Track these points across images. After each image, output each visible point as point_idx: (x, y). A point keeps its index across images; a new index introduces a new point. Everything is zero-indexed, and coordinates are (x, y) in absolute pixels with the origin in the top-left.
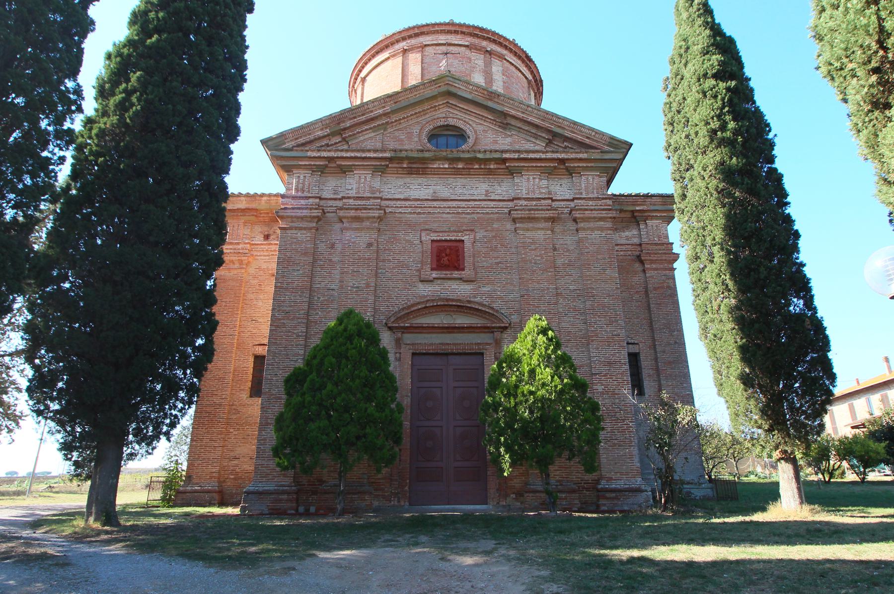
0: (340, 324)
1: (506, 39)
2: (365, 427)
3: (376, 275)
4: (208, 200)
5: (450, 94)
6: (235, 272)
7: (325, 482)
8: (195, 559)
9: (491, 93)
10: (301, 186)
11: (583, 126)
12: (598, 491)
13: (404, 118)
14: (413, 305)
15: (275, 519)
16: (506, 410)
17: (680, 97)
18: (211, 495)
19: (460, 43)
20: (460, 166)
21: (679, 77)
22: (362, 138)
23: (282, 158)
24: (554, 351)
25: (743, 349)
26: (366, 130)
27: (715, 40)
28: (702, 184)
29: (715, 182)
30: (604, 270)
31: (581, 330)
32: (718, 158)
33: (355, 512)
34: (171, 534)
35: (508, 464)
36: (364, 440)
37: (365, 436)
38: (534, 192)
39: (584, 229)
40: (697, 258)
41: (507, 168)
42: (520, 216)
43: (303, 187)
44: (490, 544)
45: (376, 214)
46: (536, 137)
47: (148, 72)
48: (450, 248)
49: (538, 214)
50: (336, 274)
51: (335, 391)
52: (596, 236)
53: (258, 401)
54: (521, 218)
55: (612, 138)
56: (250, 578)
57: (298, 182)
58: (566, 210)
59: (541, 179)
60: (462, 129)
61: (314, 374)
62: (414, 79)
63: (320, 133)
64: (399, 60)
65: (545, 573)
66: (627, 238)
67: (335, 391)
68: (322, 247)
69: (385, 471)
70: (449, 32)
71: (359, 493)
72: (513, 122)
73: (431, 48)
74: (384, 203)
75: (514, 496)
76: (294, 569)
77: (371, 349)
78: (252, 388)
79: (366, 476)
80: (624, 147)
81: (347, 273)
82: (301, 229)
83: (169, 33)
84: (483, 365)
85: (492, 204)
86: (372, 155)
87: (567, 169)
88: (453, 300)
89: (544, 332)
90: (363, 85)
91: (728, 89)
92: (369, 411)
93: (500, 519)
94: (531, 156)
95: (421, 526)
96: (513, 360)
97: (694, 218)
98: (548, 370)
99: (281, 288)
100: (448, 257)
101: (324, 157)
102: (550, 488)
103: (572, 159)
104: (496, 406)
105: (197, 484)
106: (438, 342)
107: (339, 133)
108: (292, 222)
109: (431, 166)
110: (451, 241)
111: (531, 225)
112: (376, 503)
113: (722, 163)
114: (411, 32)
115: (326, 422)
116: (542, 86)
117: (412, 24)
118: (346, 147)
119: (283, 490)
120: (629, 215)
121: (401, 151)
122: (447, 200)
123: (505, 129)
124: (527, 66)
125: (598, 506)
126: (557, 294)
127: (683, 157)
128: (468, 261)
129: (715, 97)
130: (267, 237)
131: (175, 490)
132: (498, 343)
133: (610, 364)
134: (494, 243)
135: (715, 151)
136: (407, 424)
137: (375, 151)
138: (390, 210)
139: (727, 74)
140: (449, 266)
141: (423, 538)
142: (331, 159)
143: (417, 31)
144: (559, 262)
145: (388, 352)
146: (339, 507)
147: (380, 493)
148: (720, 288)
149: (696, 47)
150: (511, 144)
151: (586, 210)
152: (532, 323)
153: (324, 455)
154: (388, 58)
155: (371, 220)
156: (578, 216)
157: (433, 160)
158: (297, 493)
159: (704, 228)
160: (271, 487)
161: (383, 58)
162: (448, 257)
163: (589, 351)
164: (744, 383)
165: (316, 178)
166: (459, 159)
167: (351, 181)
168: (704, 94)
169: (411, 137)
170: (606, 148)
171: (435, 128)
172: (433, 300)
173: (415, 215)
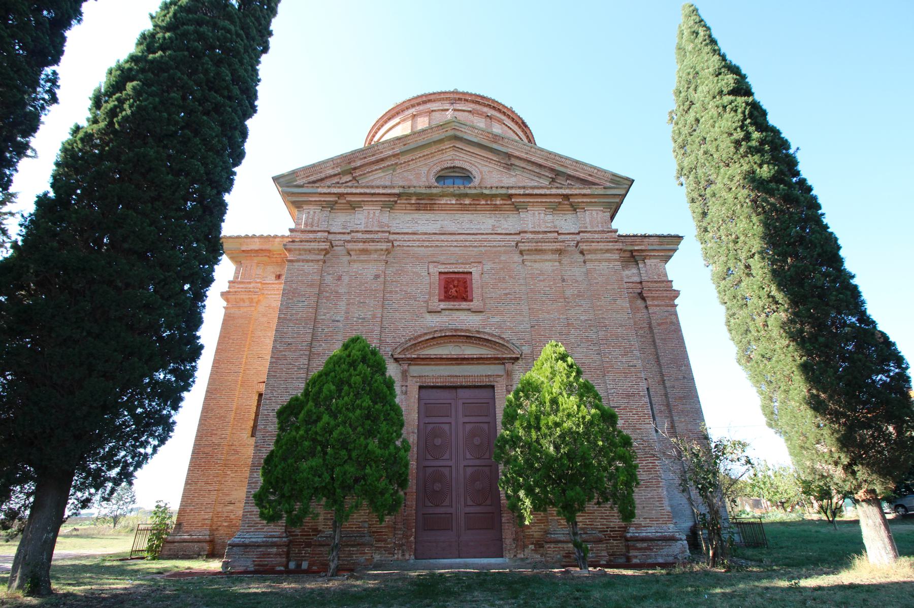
2: (364, 468)
6: (245, 310)
7: (320, 531)
10: (310, 220)
12: (627, 540)
14: (420, 336)
16: (529, 445)
18: (201, 544)
22: (372, 178)
23: (293, 194)
25: (805, 368)
26: (376, 170)
30: (615, 300)
31: (595, 362)
33: (350, 569)
35: (528, 510)
37: (364, 477)
38: (539, 226)
39: (591, 260)
40: (728, 272)
41: (513, 204)
42: (527, 248)
45: (384, 246)
46: (539, 175)
47: (146, 83)
49: (545, 246)
50: (342, 305)
51: (333, 423)
52: (606, 267)
55: (614, 175)
57: (307, 218)
58: (572, 243)
60: (468, 171)
63: (331, 172)
68: (329, 279)
69: (387, 518)
71: (358, 545)
72: (517, 162)
74: (392, 237)
77: (378, 377)
79: (366, 525)
81: (353, 304)
82: (308, 261)
86: (381, 191)
88: (461, 330)
89: (563, 358)
92: (370, 447)
93: (526, 581)
96: (530, 389)
98: (572, 398)
99: (285, 319)
100: (456, 288)
101: (334, 194)
102: (578, 539)
104: (514, 441)
105: (187, 532)
107: (350, 172)
108: (300, 254)
109: (438, 202)
111: (538, 257)
112: (377, 557)
114: (420, 100)
119: (272, 542)
120: (628, 254)
123: (509, 169)
125: (628, 559)
128: (476, 292)
130: (279, 277)
132: (509, 374)
133: (628, 396)
136: (413, 464)
140: (457, 297)
142: (340, 195)
143: (424, 99)
144: (568, 293)
145: (394, 382)
146: (333, 565)
148: (765, 301)
152: (548, 350)
158: (289, 545)
160: (259, 538)
162: (456, 288)
165: (326, 213)
166: (466, 195)
167: (360, 216)
169: (420, 175)
170: (608, 184)
171: (443, 170)
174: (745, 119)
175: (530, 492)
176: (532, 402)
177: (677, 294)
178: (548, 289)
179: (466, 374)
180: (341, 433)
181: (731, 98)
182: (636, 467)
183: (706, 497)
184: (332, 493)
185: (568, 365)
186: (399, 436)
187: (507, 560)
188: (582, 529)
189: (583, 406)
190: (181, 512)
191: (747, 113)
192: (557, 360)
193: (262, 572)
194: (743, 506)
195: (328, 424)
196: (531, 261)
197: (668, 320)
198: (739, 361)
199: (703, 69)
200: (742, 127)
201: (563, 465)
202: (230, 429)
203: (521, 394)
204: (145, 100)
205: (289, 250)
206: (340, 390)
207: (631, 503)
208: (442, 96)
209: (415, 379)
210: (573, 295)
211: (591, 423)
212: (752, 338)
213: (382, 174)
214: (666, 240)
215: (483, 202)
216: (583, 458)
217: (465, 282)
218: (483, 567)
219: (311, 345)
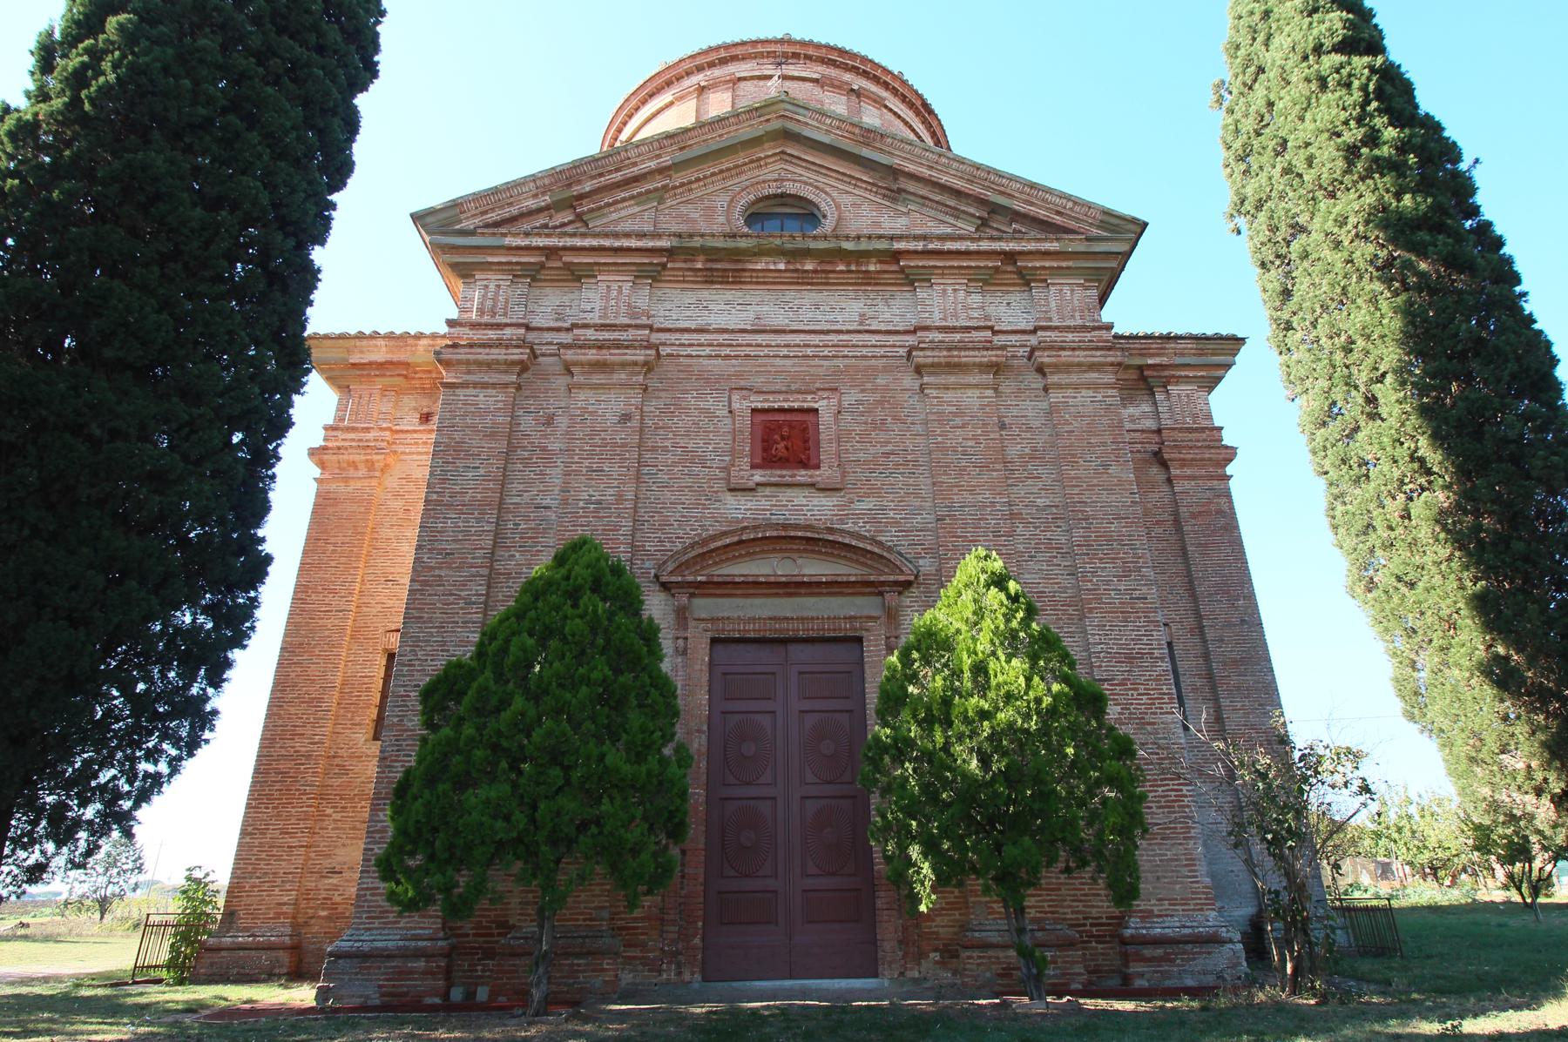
3: (638, 478)
6: (359, 485)
9: (868, 131)
10: (489, 303)
11: (1049, 191)
12: (1124, 942)
13: (698, 180)
14: (713, 538)
16: (928, 756)
18: (274, 954)
19: (804, 74)
20: (809, 267)
22: (614, 216)
24: (1026, 622)
25: (1482, 604)
26: (624, 200)
28: (1337, 258)
29: (1370, 249)
30: (1106, 466)
32: (1370, 199)
38: (955, 315)
39: (1059, 386)
41: (902, 270)
42: (932, 360)
45: (640, 356)
46: (956, 213)
48: (791, 425)
49: (966, 357)
50: (555, 475)
51: (532, 713)
52: (1087, 398)
54: (932, 365)
55: (1108, 213)
61: (488, 673)
63: (531, 203)
67: (532, 713)
68: (527, 423)
69: (647, 901)
71: (589, 953)
72: (911, 186)
73: (749, 83)
79: (605, 914)
80: (1131, 230)
81: (578, 473)
82: (485, 386)
85: (873, 339)
86: (633, 243)
87: (1020, 273)
88: (796, 527)
89: (999, 581)
92: (609, 760)
94: (949, 246)
96: (934, 644)
98: (1015, 662)
99: (439, 503)
100: (785, 441)
101: (538, 248)
102: (1027, 940)
103: (1030, 253)
104: (901, 748)
105: (246, 929)
106: (766, 613)
108: (469, 372)
110: (791, 410)
111: (952, 379)
112: (627, 978)
114: (713, 57)
119: (417, 949)
120: (1133, 375)
121: (691, 236)
122: (783, 332)
123: (894, 200)
124: (924, 122)
125: (1126, 979)
129: (1348, 85)
132: (892, 616)
133: (1130, 658)
137: (641, 235)
138: (668, 350)
139: (1363, 45)
140: (787, 460)
142: (551, 252)
143: (723, 54)
144: (1013, 451)
146: (537, 994)
148: (1406, 468)
152: (971, 567)
154: (672, 103)
155: (630, 369)
156: (1046, 360)
157: (755, 254)
158: (448, 954)
159: (1348, 350)
161: (662, 104)
162: (785, 441)
163: (1085, 632)
165: (522, 288)
166: (807, 253)
167: (591, 295)
168: (1323, 83)
169: (714, 211)
170: (1095, 232)
172: (755, 527)
174: (1367, 102)
175: (931, 848)
176: (938, 671)
177: (1230, 454)
178: (970, 443)
179: (805, 614)
181: (1338, 58)
183: (1282, 858)
185: (1009, 597)
189: (1036, 679)
191: (1371, 87)
192: (988, 586)
196: (938, 387)
201: (996, 795)
203: (915, 655)
204: (146, 53)
205: (447, 364)
207: (1132, 869)
210: (1021, 456)
211: (1053, 712)
216: (1038, 780)
217: (805, 430)
219: (492, 557)
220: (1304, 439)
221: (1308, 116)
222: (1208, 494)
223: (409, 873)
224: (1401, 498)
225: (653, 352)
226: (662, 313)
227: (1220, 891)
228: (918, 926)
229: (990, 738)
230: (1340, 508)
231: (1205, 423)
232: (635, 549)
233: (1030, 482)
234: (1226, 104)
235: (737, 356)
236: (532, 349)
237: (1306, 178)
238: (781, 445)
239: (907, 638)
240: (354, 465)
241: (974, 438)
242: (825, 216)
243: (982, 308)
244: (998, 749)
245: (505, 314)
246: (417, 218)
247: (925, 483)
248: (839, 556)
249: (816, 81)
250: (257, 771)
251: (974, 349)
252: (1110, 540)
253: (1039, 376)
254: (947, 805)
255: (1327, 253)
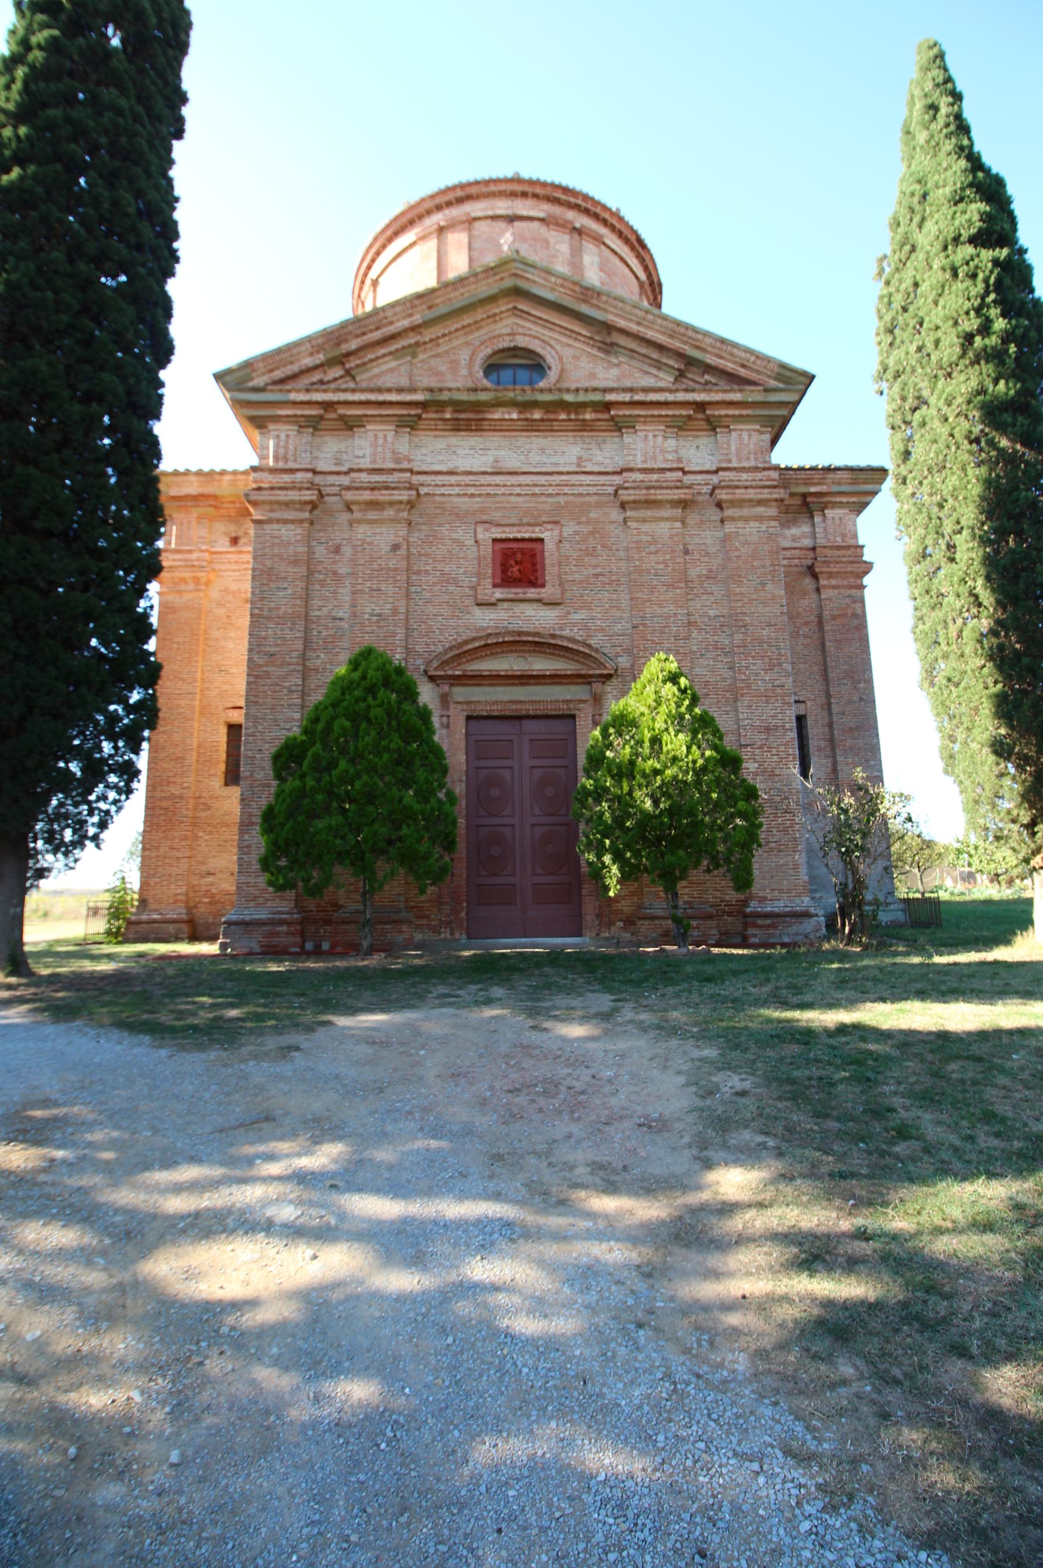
0: (355, 669)
1: (605, 208)
2: (399, 827)
3: (408, 595)
4: (128, 462)
5: (518, 293)
6: (189, 596)
8: (141, 1032)
9: (587, 289)
10: (282, 451)
11: (736, 345)
12: (746, 916)
13: (444, 335)
14: (466, 642)
15: (270, 960)
16: (619, 798)
17: (908, 283)
18: (178, 925)
21: (907, 248)
22: (376, 371)
24: (690, 709)
26: (384, 356)
27: (975, 177)
29: (965, 425)
30: (763, 584)
31: (725, 679)
32: (974, 383)
33: (388, 949)
34: (109, 988)
35: (615, 880)
36: (398, 844)
37: (400, 839)
38: (654, 458)
39: (733, 519)
41: (612, 419)
42: (632, 499)
43: (286, 453)
44: (604, 1001)
45: (404, 496)
46: (659, 365)
48: (523, 552)
50: (345, 594)
51: (352, 771)
52: (753, 530)
53: (235, 791)
54: (634, 502)
55: (784, 366)
56: (224, 1066)
57: (277, 446)
58: (706, 489)
59: (665, 438)
60: (538, 355)
61: (318, 745)
62: (459, 264)
63: (308, 361)
64: (432, 244)
65: (710, 1052)
66: (794, 539)
67: (352, 771)
68: (321, 552)
69: (431, 890)
70: (513, 195)
71: (393, 922)
72: (622, 340)
74: (416, 479)
75: (620, 924)
76: (297, 1049)
77: (406, 706)
78: (227, 772)
79: (402, 898)
80: (800, 381)
81: (362, 592)
82: (285, 522)
83: (40, 164)
84: (574, 733)
85: (588, 479)
86: (394, 397)
87: (708, 420)
88: (528, 634)
89: (673, 678)
90: (375, 291)
91: (996, 262)
93: (606, 959)
95: (489, 971)
96: (624, 723)
97: (926, 489)
98: (681, 736)
99: (260, 616)
100: (519, 565)
101: (317, 403)
103: (717, 403)
104: (599, 794)
105: (155, 910)
106: (506, 698)
107: (339, 361)
108: (272, 511)
110: (523, 540)
111: (648, 513)
112: (418, 937)
113: (982, 391)
114: (451, 196)
115: (340, 818)
116: (661, 292)
117: (451, 182)
118: (352, 385)
120: (797, 501)
121: (441, 390)
123: (607, 352)
124: (639, 256)
125: (745, 938)
126: (690, 624)
127: (911, 386)
128: (550, 573)
129: (974, 276)
130: (235, 541)
131: (128, 921)
132: (598, 700)
133: (768, 730)
134: (591, 542)
135: (970, 370)
136: (462, 822)
137: (400, 390)
139: (995, 236)
140: (520, 580)
141: (498, 992)
142: (328, 405)
143: (459, 193)
144: (693, 572)
146: (365, 944)
147: (424, 922)
148: (965, 601)
149: (941, 191)
150: (618, 379)
151: (738, 487)
152: (655, 666)
153: (338, 869)
154: (413, 245)
155: (396, 507)
156: (724, 497)
157: (493, 406)
158: (302, 922)
159: (941, 506)
160: (263, 915)
161: (406, 244)
162: (519, 565)
163: (736, 711)
164: (996, 753)
165: (306, 437)
166: (535, 405)
167: (362, 442)
169: (456, 366)
170: (773, 383)
171: (495, 353)
172: (497, 634)
173: (467, 499)
174: (987, 293)
175: (618, 857)
176: (627, 742)
177: (868, 567)
178: (661, 566)
179: (534, 698)
180: (365, 785)
181: (970, 250)
182: (760, 826)
183: (851, 862)
184: (358, 860)
185: (680, 689)
186: (442, 786)
187: (587, 940)
188: (686, 903)
189: (694, 747)
190: (144, 885)
191: (992, 280)
192: (664, 682)
193: (275, 953)
194: (942, 878)
195: (347, 772)
197: (849, 611)
198: (921, 687)
199: (937, 187)
200: (978, 311)
201: (662, 823)
202: (193, 775)
203: (611, 730)
204: (16, 269)
205: (254, 504)
206: (356, 727)
207: (748, 871)
208: (492, 188)
209: (460, 707)
210: (699, 576)
211: (704, 769)
212: (940, 655)
213: (393, 364)
214: (862, 476)
215: (563, 416)
216: (691, 813)
217: (534, 556)
218: (556, 946)
219: (304, 657)
220: (906, 570)
221: (941, 302)
222: (847, 600)
223: (280, 869)
224: (959, 621)
225: (414, 493)
226: (419, 458)
227: (814, 885)
228: (609, 905)
229: (660, 787)
230: (921, 627)
231: (852, 542)
232: (408, 650)
233: (705, 597)
234: (884, 277)
235: (480, 495)
236: (319, 491)
237: (933, 357)
238: (515, 569)
239: (607, 718)
240: (184, 580)
241: (665, 562)
242: (550, 368)
243: (676, 451)
244: (663, 794)
245: (295, 461)
246: (219, 377)
247: (624, 597)
248: (559, 656)
249: (542, 220)
250: (147, 808)
251: (667, 488)
252: (761, 642)
253: (718, 510)
254: (629, 829)
255: (937, 424)
